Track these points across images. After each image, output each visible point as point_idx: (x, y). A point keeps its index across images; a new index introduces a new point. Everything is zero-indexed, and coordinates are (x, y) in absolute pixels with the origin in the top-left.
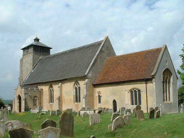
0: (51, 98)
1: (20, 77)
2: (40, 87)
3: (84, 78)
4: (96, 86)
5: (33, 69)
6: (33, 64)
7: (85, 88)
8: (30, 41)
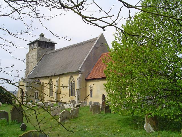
0: (51, 92)
1: (26, 71)
2: (42, 81)
3: (78, 73)
4: (88, 80)
5: (37, 64)
6: (38, 59)
7: (78, 83)
8: (37, 37)
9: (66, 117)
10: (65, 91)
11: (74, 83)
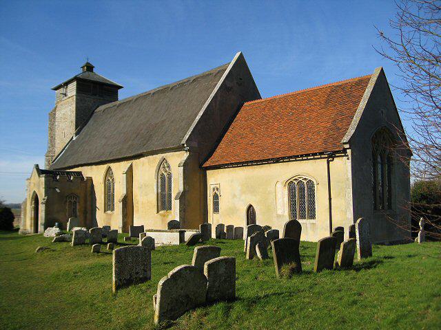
5: (76, 134)
9: (187, 296)
10: (145, 198)
11: (170, 179)
